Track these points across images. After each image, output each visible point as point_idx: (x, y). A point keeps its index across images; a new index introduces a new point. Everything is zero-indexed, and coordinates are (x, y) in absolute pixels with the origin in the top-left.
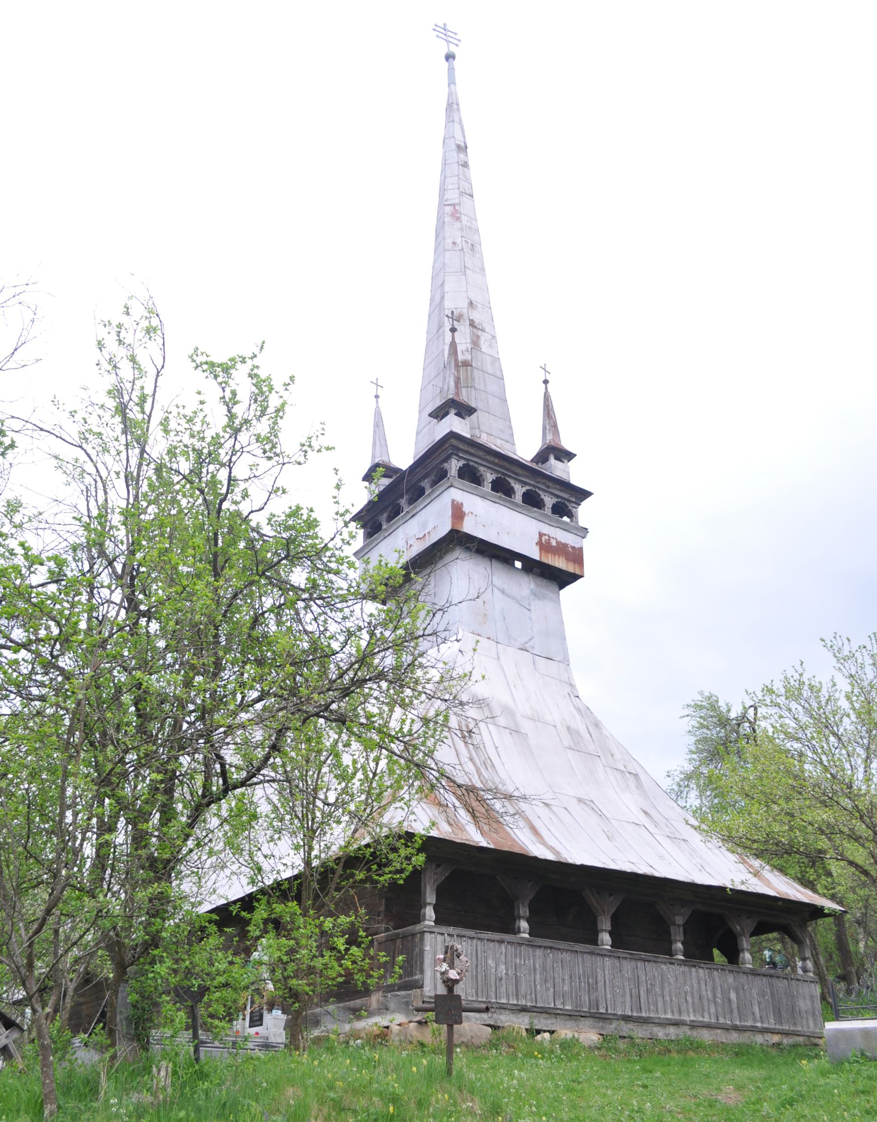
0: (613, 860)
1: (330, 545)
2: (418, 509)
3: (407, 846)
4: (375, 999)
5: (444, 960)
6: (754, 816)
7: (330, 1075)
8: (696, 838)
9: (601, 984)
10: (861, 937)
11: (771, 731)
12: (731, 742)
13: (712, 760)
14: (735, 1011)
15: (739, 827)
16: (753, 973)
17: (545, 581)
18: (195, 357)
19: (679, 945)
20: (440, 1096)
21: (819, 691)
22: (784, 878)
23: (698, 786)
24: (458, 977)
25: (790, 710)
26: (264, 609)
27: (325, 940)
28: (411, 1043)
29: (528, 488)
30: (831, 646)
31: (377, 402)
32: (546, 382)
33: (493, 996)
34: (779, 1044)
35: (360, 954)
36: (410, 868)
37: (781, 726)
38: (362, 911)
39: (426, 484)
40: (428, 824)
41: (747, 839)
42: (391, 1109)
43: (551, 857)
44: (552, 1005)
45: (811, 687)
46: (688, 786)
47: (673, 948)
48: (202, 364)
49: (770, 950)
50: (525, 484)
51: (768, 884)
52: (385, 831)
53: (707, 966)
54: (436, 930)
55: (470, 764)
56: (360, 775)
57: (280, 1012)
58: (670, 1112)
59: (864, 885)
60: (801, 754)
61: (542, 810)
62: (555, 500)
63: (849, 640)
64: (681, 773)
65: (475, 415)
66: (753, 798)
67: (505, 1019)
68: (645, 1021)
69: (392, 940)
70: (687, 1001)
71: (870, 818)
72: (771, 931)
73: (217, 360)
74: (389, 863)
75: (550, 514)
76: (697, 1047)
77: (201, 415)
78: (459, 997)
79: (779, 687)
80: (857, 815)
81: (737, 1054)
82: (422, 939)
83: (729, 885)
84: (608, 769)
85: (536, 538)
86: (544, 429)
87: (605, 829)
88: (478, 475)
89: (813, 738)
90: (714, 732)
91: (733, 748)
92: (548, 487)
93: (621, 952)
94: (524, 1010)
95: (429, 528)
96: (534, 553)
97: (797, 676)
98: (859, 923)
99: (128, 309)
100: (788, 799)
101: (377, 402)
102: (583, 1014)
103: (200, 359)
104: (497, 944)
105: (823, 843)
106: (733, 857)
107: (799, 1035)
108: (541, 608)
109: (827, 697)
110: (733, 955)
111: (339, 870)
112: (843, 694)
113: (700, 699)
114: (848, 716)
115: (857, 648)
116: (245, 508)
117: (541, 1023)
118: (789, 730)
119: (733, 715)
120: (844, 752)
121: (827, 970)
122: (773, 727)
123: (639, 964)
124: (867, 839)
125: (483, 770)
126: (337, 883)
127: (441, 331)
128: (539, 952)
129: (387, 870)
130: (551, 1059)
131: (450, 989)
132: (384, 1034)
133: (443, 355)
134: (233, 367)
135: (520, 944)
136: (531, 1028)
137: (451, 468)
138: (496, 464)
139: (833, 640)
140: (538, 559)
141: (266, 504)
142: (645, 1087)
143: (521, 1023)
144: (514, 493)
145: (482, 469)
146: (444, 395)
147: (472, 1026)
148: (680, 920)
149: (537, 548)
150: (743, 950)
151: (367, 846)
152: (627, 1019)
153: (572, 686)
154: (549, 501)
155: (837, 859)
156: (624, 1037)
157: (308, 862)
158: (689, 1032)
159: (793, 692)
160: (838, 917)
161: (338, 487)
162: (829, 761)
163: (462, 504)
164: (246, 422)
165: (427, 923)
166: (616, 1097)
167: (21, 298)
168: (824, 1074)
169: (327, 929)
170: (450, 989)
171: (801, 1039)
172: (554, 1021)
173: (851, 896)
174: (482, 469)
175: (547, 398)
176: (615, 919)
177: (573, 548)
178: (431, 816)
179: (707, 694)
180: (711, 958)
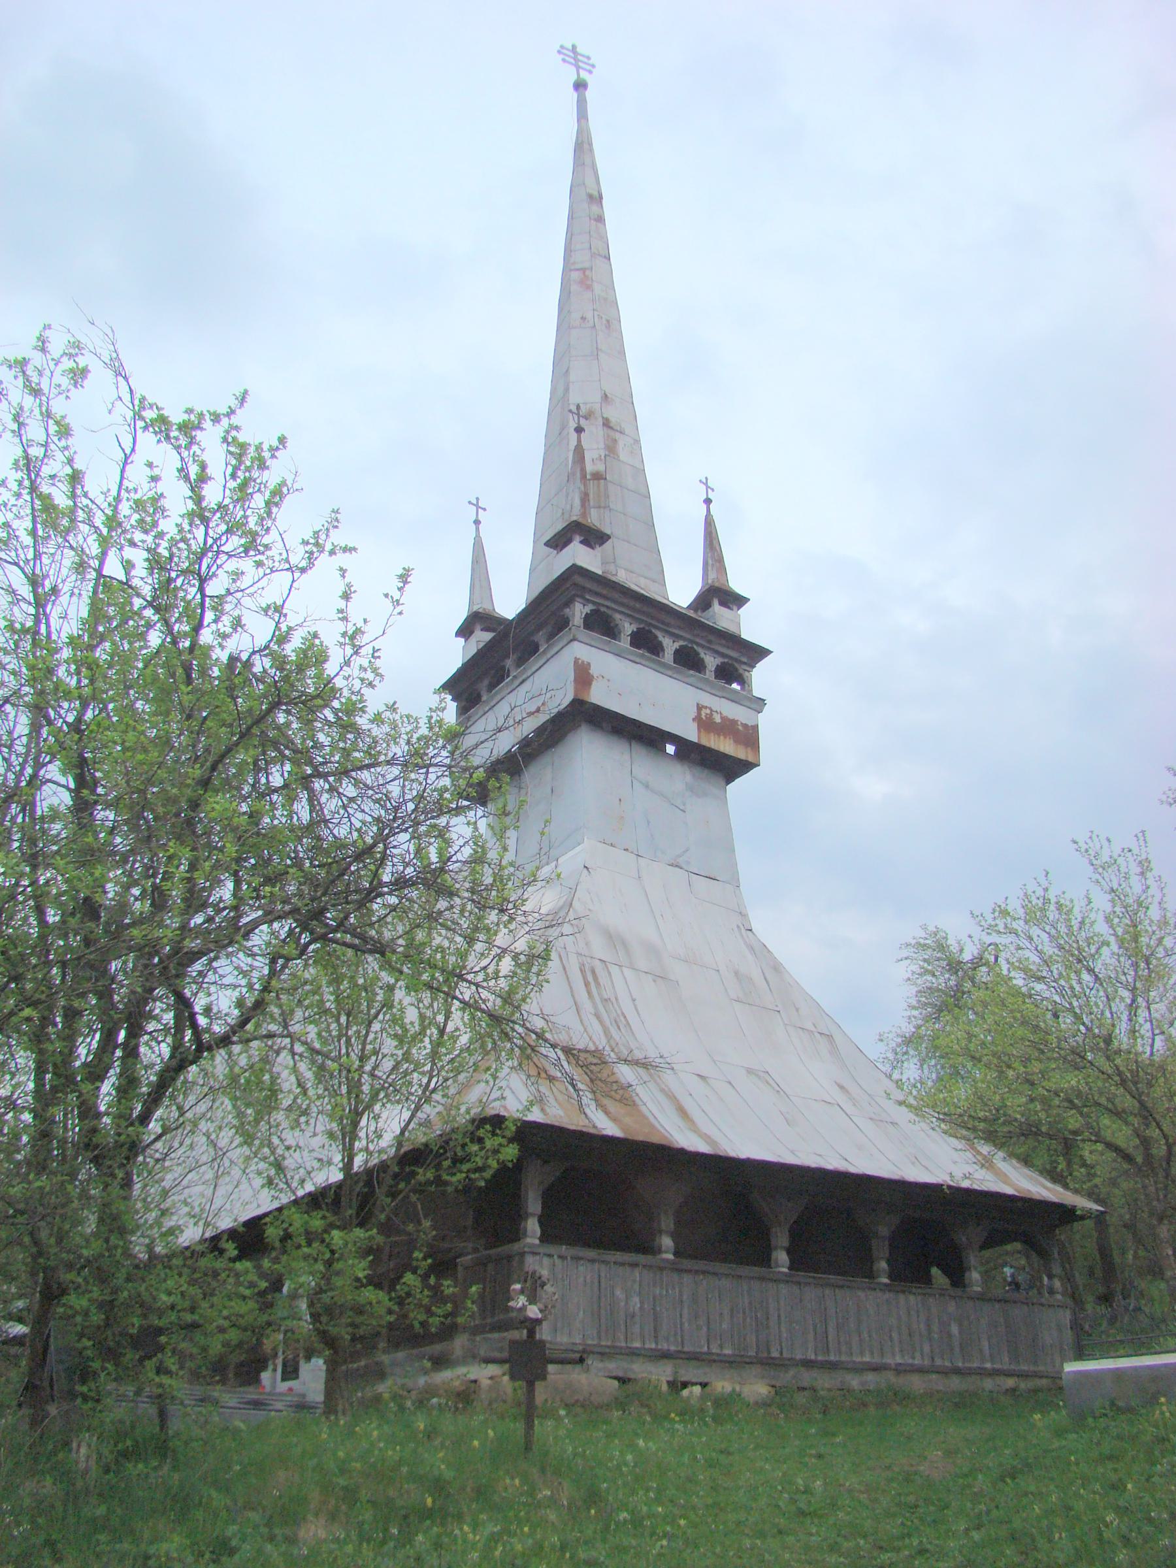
0: (792, 1152)
2: (529, 673)
3: (494, 1134)
14: (957, 1350)
16: (982, 1298)
17: (706, 771)
19: (883, 1265)
21: (1070, 911)
22: (1026, 1171)
24: (540, 1316)
25: (1030, 939)
29: (682, 643)
30: (1087, 851)
31: (477, 530)
32: (708, 501)
33: (622, 1337)
34: (1014, 1390)
36: (495, 1165)
38: (427, 1223)
39: (540, 637)
43: (703, 1148)
44: (705, 1349)
45: (1059, 907)
47: (875, 1268)
50: (676, 637)
51: (1005, 1178)
53: (920, 1291)
54: (541, 1250)
55: (595, 1022)
58: (850, 1491)
63: (1108, 840)
67: (639, 1369)
68: (833, 1366)
69: (483, 1263)
71: (1135, 1083)
72: (1002, 1242)
74: (466, 1158)
75: (712, 678)
76: (903, 1398)
79: (1015, 906)
81: (956, 1405)
85: (693, 712)
86: (705, 564)
92: (710, 642)
94: (665, 1356)
96: (690, 733)
97: (1040, 892)
99: (44, 342)
101: (477, 530)
102: (747, 1360)
104: (628, 1268)
105: (1074, 1121)
107: (1041, 1377)
109: (1079, 919)
110: (957, 1276)
112: (1101, 913)
113: (924, 935)
115: (1119, 851)
117: (689, 1372)
119: (966, 957)
122: (1008, 963)
123: (827, 1292)
125: (613, 1031)
126: (391, 1186)
127: (565, 432)
128: (687, 1278)
132: (466, 1396)
133: (566, 465)
135: (661, 1269)
138: (639, 611)
139: (1089, 841)
140: (696, 741)
142: (820, 1456)
143: (660, 1374)
144: (663, 650)
145: (617, 616)
146: (566, 516)
148: (884, 1231)
149: (695, 726)
152: (808, 1364)
153: (743, 915)
154: (711, 662)
155: (1091, 1141)
156: (804, 1389)
159: (1035, 914)
160: (1100, 1218)
161: (346, 596)
163: (589, 664)
165: (529, 1240)
168: (1059, 1433)
171: (1044, 1381)
174: (617, 616)
175: (709, 523)
177: (745, 726)
179: (932, 928)
180: (927, 1280)
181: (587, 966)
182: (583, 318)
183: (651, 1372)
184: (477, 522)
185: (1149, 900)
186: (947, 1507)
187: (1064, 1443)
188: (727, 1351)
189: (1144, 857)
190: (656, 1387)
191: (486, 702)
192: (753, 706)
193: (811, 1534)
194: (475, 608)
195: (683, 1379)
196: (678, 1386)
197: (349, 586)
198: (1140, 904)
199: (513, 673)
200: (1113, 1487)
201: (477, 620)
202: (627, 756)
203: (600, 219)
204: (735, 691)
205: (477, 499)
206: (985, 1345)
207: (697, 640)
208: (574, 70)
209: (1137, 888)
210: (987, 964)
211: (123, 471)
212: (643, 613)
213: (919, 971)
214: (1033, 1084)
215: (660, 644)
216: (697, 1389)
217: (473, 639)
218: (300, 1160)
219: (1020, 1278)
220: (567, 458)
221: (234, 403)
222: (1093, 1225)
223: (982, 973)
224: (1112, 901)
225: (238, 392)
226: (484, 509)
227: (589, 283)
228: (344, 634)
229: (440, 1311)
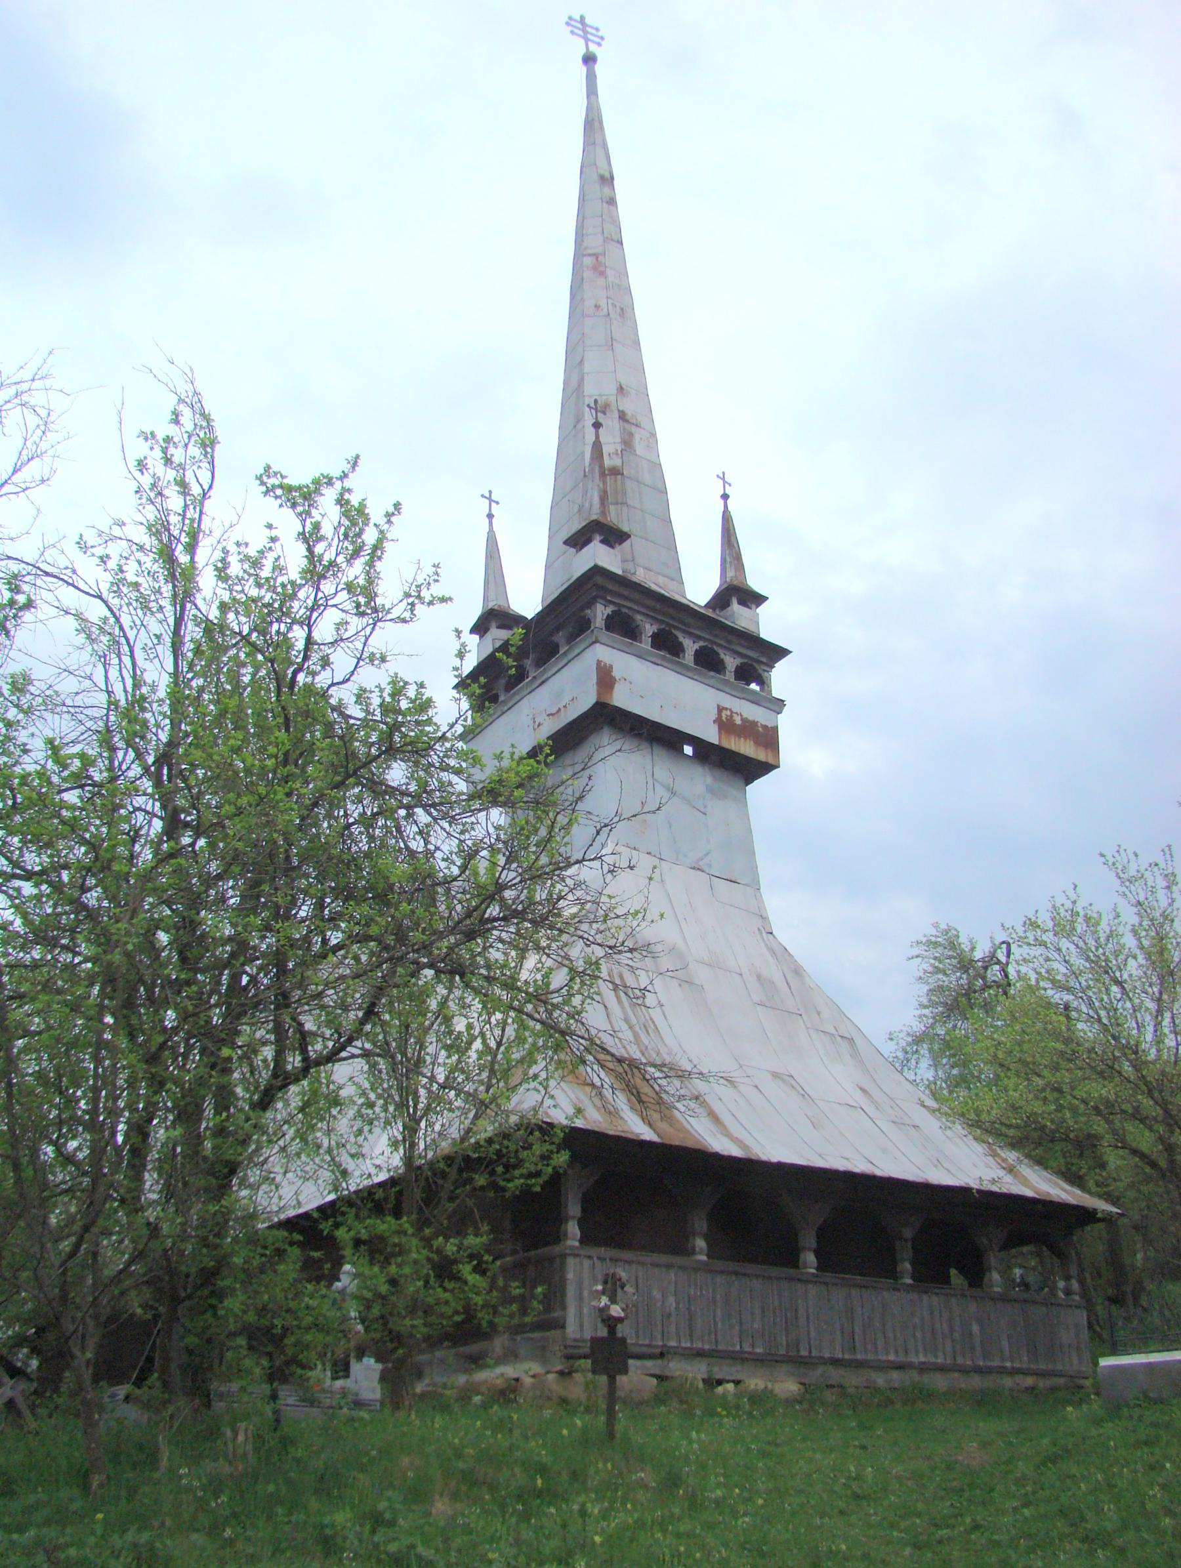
1: (449, 735)
4: (499, 1344)
5: (603, 1292)
6: (1011, 1093)
7: (456, 1441)
8: (931, 1124)
9: (802, 1321)
10: (1138, 1246)
11: (1033, 977)
12: (975, 992)
13: (949, 1016)
15: (992, 1108)
16: (1004, 1299)
18: (265, 479)
20: (600, 1465)
21: (1097, 924)
22: (1045, 1173)
23: (931, 1050)
24: (622, 1315)
25: (1059, 950)
26: (351, 820)
27: (444, 1270)
28: (550, 1399)
29: (701, 643)
30: (1114, 864)
31: (491, 524)
32: (725, 497)
33: (659, 1337)
35: (484, 1285)
36: (550, 1169)
37: (1047, 972)
39: (560, 637)
40: (571, 1111)
41: (1002, 1124)
42: (539, 1482)
43: (736, 1152)
44: (738, 1348)
45: (1087, 919)
46: (917, 1051)
48: (274, 487)
49: (1021, 1266)
50: (697, 638)
51: (1026, 1182)
52: (514, 1119)
54: (582, 1252)
56: (478, 1045)
57: (372, 1360)
58: (897, 1477)
59: (1148, 1179)
60: (1067, 1007)
61: (724, 1091)
62: (738, 661)
63: (1136, 855)
64: (908, 1034)
65: (627, 544)
66: (1009, 1069)
68: (861, 1365)
70: (914, 1336)
71: (1161, 1091)
72: (1022, 1244)
73: (292, 481)
74: (520, 1163)
75: (732, 680)
76: (929, 1396)
77: (271, 557)
78: (623, 1340)
79: (1045, 919)
80: (1144, 1088)
82: (563, 1264)
83: (974, 1185)
84: (812, 1032)
87: (810, 1114)
88: (633, 625)
89: (1089, 987)
90: (953, 978)
91: (979, 998)
92: (729, 642)
93: (829, 1276)
94: (700, 1354)
95: (566, 700)
96: (711, 735)
97: (1068, 905)
98: (1136, 1228)
99: (177, 416)
100: (1056, 1068)
101: (491, 524)
102: (778, 1359)
103: (271, 482)
105: (1099, 1126)
106: (979, 1148)
108: (720, 810)
110: (976, 1277)
111: (453, 1174)
112: (1129, 927)
113: (934, 932)
114: (1135, 957)
116: (323, 680)
118: (1058, 978)
119: (978, 955)
120: (1128, 1005)
121: (1095, 1290)
122: (1037, 973)
123: (854, 1291)
124: (1155, 1119)
125: (643, 1036)
127: (579, 426)
128: (720, 1280)
129: (517, 1173)
130: (739, 1417)
131: (612, 1330)
132: (508, 1393)
133: (583, 459)
134: (317, 491)
135: (696, 1270)
136: (709, 1378)
137: (595, 616)
138: (655, 610)
139: (1116, 855)
141: (352, 673)
142: (864, 1447)
143: (696, 1371)
145: (639, 617)
147: (637, 1378)
148: (908, 1233)
149: (715, 728)
150: (989, 1270)
151: (490, 1141)
152: (835, 1362)
153: (764, 918)
154: (731, 663)
155: (1117, 1147)
156: (832, 1386)
157: (408, 1160)
158: (917, 1378)
159: (1064, 928)
162: (1109, 1017)
163: (611, 667)
164: (332, 564)
165: (569, 1243)
166: (826, 1462)
167: (25, 398)
168: (1098, 1422)
169: (450, 1253)
170: (612, 1330)
171: (1062, 1380)
172: (739, 1368)
173: (1131, 1194)
174: (639, 617)
176: (821, 1234)
177: (765, 727)
178: (575, 1100)
179: (943, 926)
180: (946, 1280)
181: (615, 971)
182: (597, 307)
184: (490, 516)
185: (1175, 913)
187: (1101, 1431)
188: (759, 1350)
189: (1170, 871)
193: (870, 1515)
194: (490, 605)
195: (718, 1377)
196: (712, 1383)
198: (1166, 918)
199: (532, 675)
200: (1152, 1468)
201: (494, 618)
202: (649, 757)
203: (612, 202)
204: (753, 692)
205: (490, 492)
206: (1005, 1344)
208: (582, 42)
209: (1163, 902)
210: (998, 962)
212: (663, 614)
213: (930, 969)
215: (681, 644)
216: (730, 1387)
217: (489, 637)
220: (583, 453)
221: (347, 467)
223: (994, 973)
224: (1139, 914)
225: (350, 455)
226: (497, 503)
227: (602, 269)
229: (506, 1312)
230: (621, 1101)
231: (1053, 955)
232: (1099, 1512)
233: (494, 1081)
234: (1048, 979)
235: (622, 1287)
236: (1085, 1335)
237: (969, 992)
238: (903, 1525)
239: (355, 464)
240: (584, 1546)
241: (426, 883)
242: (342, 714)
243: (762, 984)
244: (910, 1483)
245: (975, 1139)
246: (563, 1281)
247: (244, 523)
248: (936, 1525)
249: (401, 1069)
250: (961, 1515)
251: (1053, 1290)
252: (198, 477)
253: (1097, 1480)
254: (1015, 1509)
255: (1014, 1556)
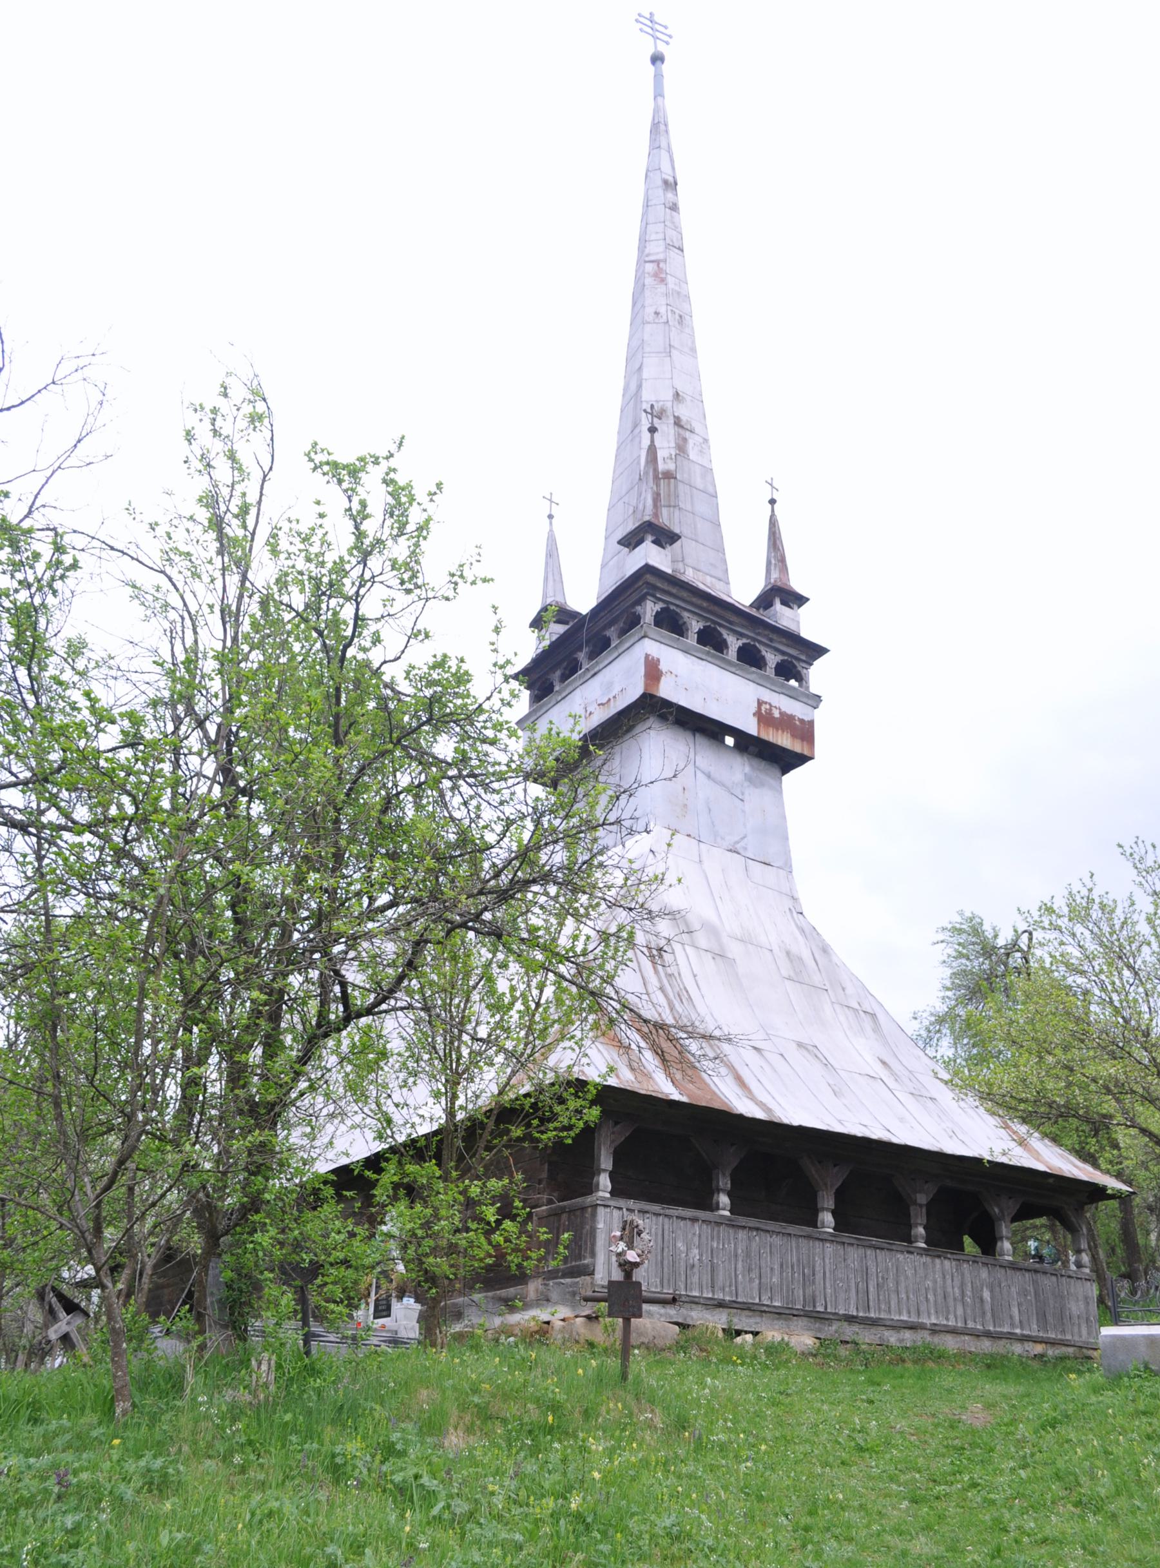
0: (840, 1121)
2: (601, 666)
4: (533, 1288)
5: (621, 1239)
6: (1022, 1068)
7: (473, 1376)
8: (946, 1096)
9: (819, 1276)
12: (997, 977)
14: (989, 1315)
16: (1014, 1267)
17: (764, 763)
19: (921, 1230)
21: (1113, 911)
24: (638, 1260)
25: (1074, 935)
28: (577, 1342)
29: (745, 641)
30: (1131, 855)
33: (683, 1287)
34: (1042, 1356)
39: (612, 632)
40: (604, 1070)
42: (550, 1418)
43: (760, 1115)
44: (757, 1301)
45: (1103, 907)
46: (939, 1031)
47: (913, 1233)
48: (321, 464)
49: (1036, 1239)
50: (741, 635)
51: (1037, 1156)
52: (550, 1077)
53: (955, 1257)
56: (519, 1006)
62: (779, 658)
63: (1154, 847)
64: (932, 1014)
65: (677, 544)
67: (697, 1316)
68: (874, 1323)
70: (927, 1300)
74: (554, 1117)
75: (773, 675)
76: (939, 1356)
78: (639, 1284)
79: (1061, 905)
84: (837, 1007)
86: (769, 563)
87: (831, 1082)
88: (681, 622)
90: (976, 963)
92: (771, 640)
93: (846, 1237)
94: (721, 1305)
96: (751, 727)
97: (1084, 892)
99: (225, 388)
100: (1066, 1049)
102: (795, 1313)
103: (319, 458)
104: (689, 1223)
105: (1109, 1106)
106: (992, 1121)
108: (758, 798)
109: (1122, 919)
110: (988, 1245)
111: (491, 1124)
112: (1144, 916)
113: (959, 920)
114: (1149, 944)
116: (376, 656)
117: (742, 1321)
119: (1001, 942)
122: (1051, 956)
123: (869, 1252)
127: (637, 431)
128: (742, 1234)
129: (551, 1126)
131: (628, 1275)
133: (639, 463)
135: (718, 1224)
136: (730, 1328)
137: (645, 613)
139: (1134, 846)
142: (871, 1402)
143: (717, 1321)
144: (727, 648)
145: (685, 614)
146: (639, 516)
147: (654, 1322)
148: (922, 1199)
150: (1001, 1238)
152: (850, 1319)
153: (794, 899)
154: (772, 659)
156: (847, 1342)
157: (450, 1113)
158: (929, 1339)
159: (1079, 912)
160: (1124, 1200)
161: (497, 630)
163: (658, 660)
164: (379, 542)
165: (601, 1194)
167: (86, 372)
168: (1097, 1390)
170: (628, 1275)
171: (1071, 1350)
172: (758, 1319)
174: (685, 614)
175: (773, 523)
177: (802, 721)
178: (610, 1060)
179: (968, 914)
180: (960, 1247)
183: (707, 1320)
186: (992, 1450)
187: (1101, 1398)
190: (713, 1333)
191: (559, 692)
192: (810, 702)
197: (500, 621)
202: (692, 745)
204: (793, 688)
206: (1015, 1311)
207: (759, 638)
210: (1020, 950)
211: (262, 488)
213: (954, 954)
214: (1071, 1070)
215: (725, 641)
216: (749, 1337)
218: (407, 1117)
219: (1045, 1252)
220: (639, 456)
222: (1117, 1205)
223: (1017, 959)
228: (495, 665)
230: (650, 1060)
231: (1068, 939)
232: (1093, 1477)
233: (531, 1038)
234: (1062, 962)
235: (639, 1234)
236: (1094, 1306)
237: (990, 977)
238: (902, 1478)
239: (401, 444)
240: (582, 1481)
241: (470, 847)
242: (393, 690)
243: (791, 961)
244: (913, 1438)
245: (987, 1110)
246: (593, 1231)
247: (297, 503)
248: (935, 1481)
249: (444, 1028)
250: (960, 1473)
251: (1066, 1263)
252: (252, 449)
253: (1093, 1446)
254: (1013, 1470)
255: (1007, 1516)
